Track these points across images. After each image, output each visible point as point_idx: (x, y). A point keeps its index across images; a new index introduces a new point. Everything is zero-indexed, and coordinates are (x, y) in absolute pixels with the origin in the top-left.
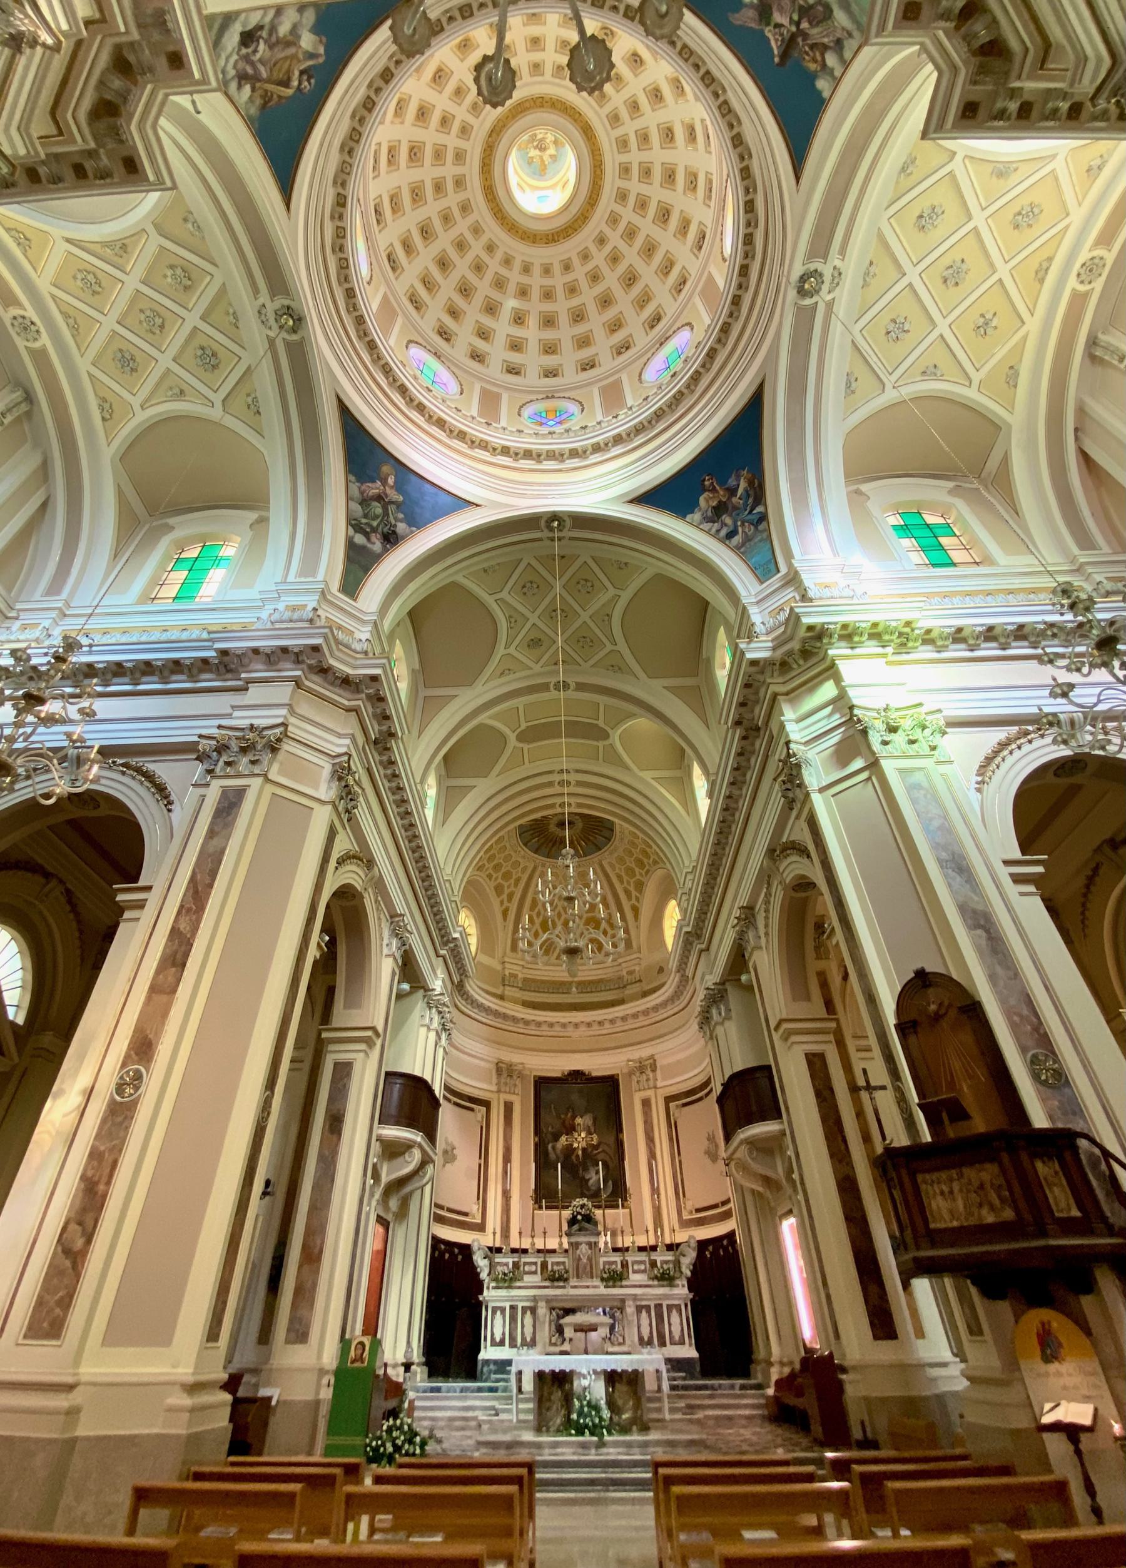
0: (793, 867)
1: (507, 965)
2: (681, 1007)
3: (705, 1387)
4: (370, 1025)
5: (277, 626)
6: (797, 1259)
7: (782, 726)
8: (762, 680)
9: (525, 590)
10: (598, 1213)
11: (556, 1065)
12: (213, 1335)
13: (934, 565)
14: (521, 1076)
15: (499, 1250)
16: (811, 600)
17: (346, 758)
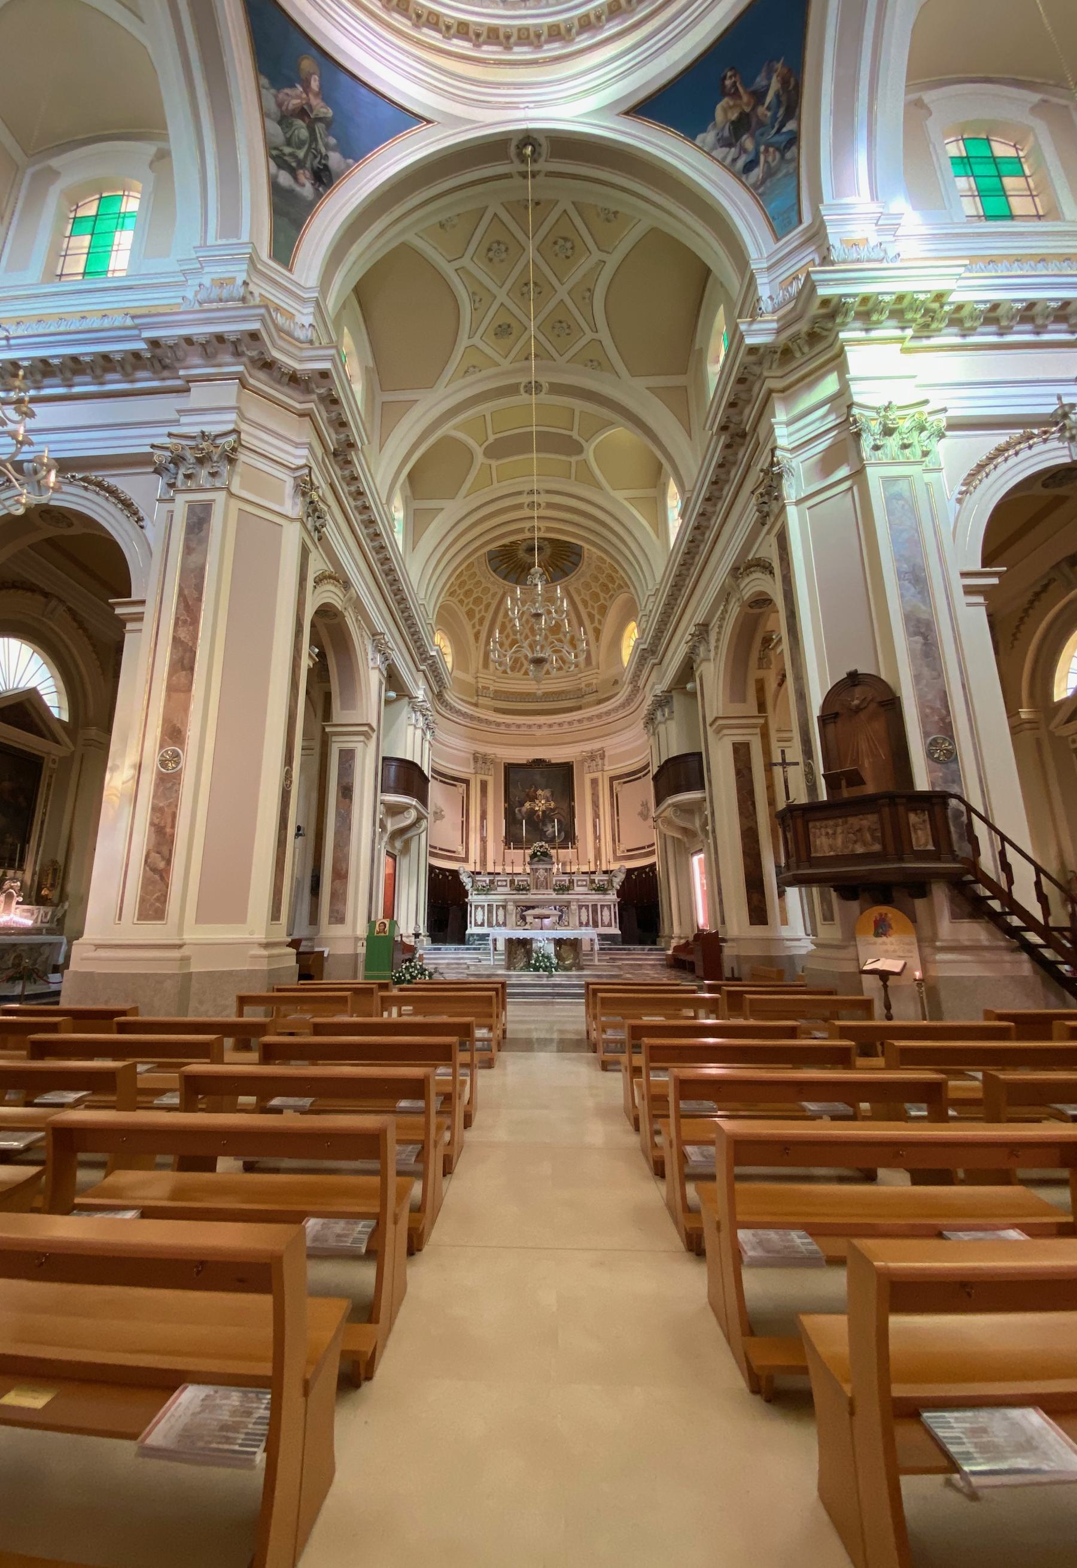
0: (755, 584)
1: (480, 680)
2: (631, 710)
3: (624, 949)
4: (365, 722)
5: (206, 306)
6: (701, 880)
7: (771, 430)
8: (758, 373)
9: (491, 254)
10: (553, 852)
11: (523, 755)
12: (275, 915)
13: (987, 218)
14: (492, 762)
15: (479, 873)
16: (833, 263)
17: (306, 471)
